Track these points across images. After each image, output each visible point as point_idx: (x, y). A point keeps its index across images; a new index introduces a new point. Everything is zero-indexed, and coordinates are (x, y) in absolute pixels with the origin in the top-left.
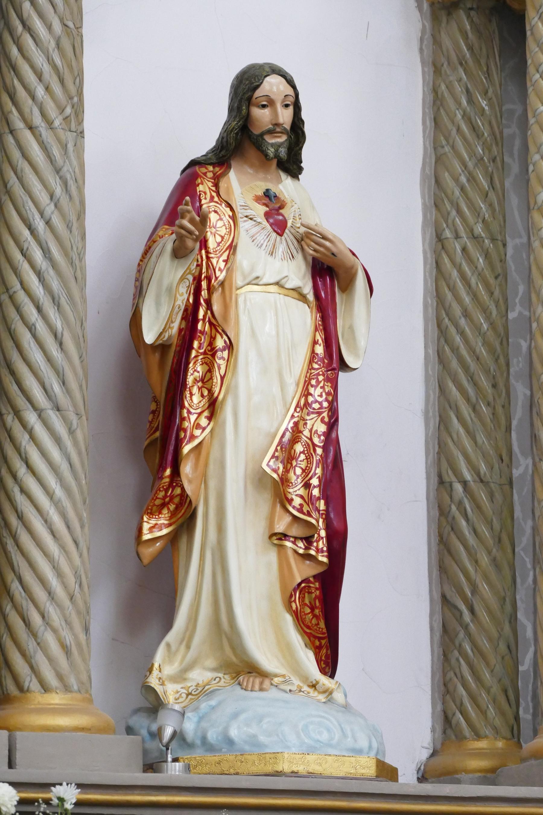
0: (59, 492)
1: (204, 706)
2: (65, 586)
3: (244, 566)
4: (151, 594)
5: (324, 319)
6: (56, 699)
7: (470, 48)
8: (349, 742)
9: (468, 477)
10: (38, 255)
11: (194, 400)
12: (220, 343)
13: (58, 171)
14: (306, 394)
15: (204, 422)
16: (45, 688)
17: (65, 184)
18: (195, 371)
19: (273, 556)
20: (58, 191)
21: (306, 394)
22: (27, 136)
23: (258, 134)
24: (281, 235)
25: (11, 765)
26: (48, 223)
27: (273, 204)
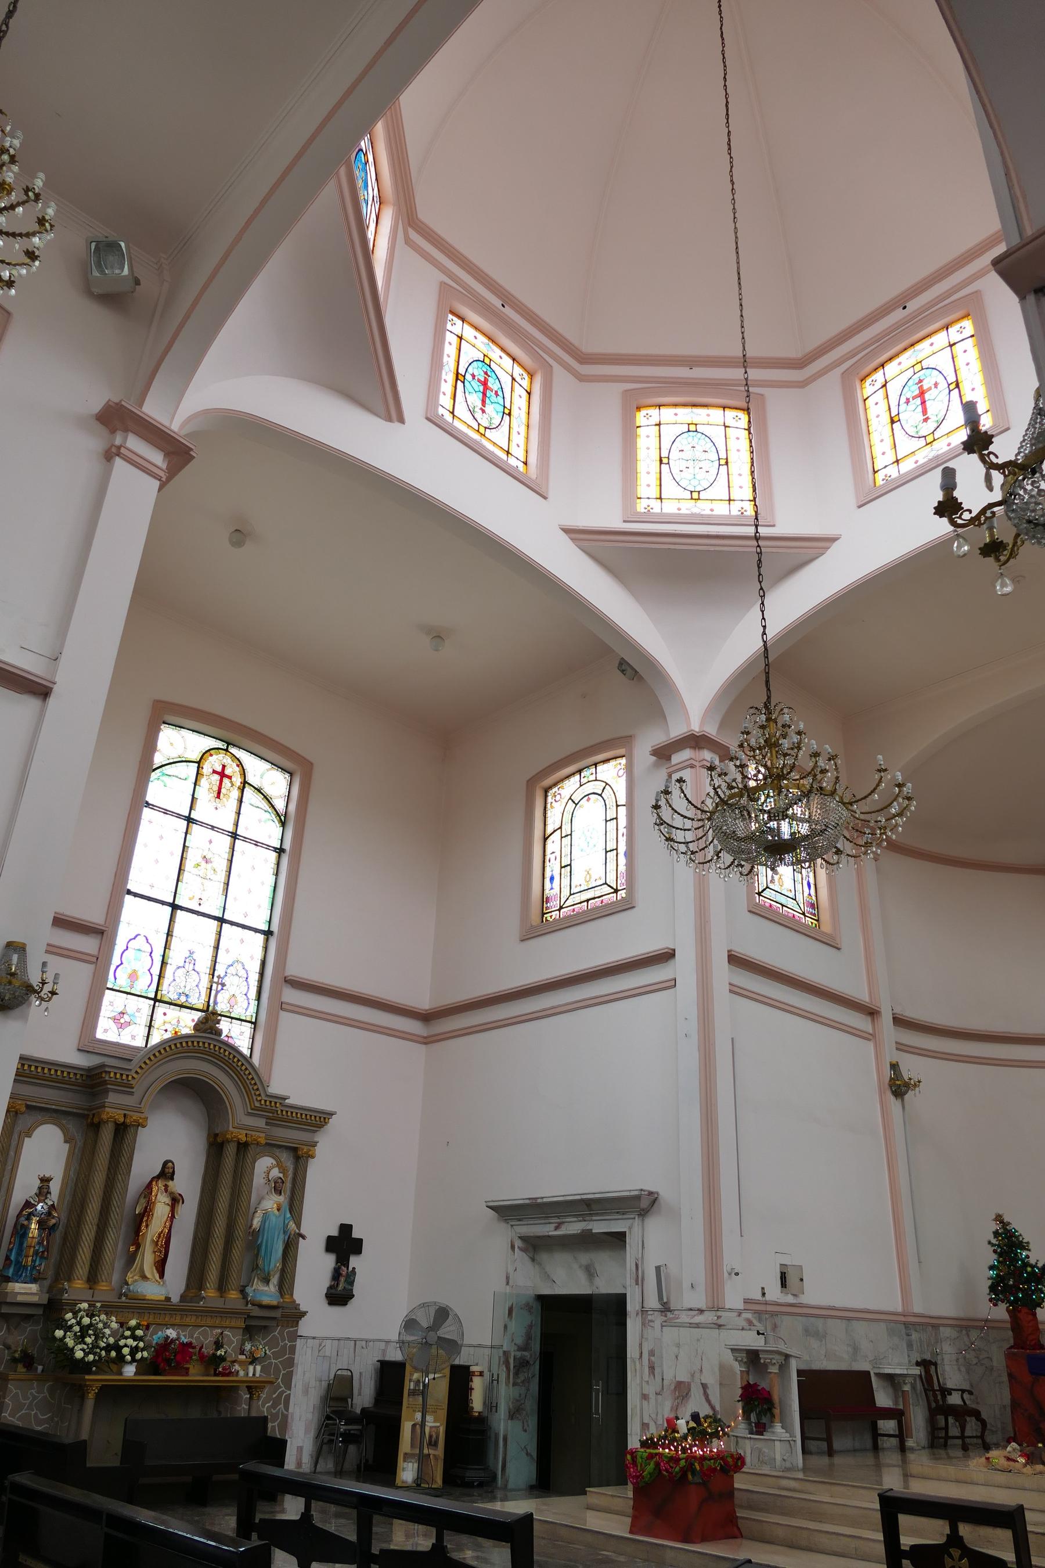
3: (148, 1258)
4: (131, 1259)
23: (167, 1173)
24: (617, 1304)
27: (166, 1186)
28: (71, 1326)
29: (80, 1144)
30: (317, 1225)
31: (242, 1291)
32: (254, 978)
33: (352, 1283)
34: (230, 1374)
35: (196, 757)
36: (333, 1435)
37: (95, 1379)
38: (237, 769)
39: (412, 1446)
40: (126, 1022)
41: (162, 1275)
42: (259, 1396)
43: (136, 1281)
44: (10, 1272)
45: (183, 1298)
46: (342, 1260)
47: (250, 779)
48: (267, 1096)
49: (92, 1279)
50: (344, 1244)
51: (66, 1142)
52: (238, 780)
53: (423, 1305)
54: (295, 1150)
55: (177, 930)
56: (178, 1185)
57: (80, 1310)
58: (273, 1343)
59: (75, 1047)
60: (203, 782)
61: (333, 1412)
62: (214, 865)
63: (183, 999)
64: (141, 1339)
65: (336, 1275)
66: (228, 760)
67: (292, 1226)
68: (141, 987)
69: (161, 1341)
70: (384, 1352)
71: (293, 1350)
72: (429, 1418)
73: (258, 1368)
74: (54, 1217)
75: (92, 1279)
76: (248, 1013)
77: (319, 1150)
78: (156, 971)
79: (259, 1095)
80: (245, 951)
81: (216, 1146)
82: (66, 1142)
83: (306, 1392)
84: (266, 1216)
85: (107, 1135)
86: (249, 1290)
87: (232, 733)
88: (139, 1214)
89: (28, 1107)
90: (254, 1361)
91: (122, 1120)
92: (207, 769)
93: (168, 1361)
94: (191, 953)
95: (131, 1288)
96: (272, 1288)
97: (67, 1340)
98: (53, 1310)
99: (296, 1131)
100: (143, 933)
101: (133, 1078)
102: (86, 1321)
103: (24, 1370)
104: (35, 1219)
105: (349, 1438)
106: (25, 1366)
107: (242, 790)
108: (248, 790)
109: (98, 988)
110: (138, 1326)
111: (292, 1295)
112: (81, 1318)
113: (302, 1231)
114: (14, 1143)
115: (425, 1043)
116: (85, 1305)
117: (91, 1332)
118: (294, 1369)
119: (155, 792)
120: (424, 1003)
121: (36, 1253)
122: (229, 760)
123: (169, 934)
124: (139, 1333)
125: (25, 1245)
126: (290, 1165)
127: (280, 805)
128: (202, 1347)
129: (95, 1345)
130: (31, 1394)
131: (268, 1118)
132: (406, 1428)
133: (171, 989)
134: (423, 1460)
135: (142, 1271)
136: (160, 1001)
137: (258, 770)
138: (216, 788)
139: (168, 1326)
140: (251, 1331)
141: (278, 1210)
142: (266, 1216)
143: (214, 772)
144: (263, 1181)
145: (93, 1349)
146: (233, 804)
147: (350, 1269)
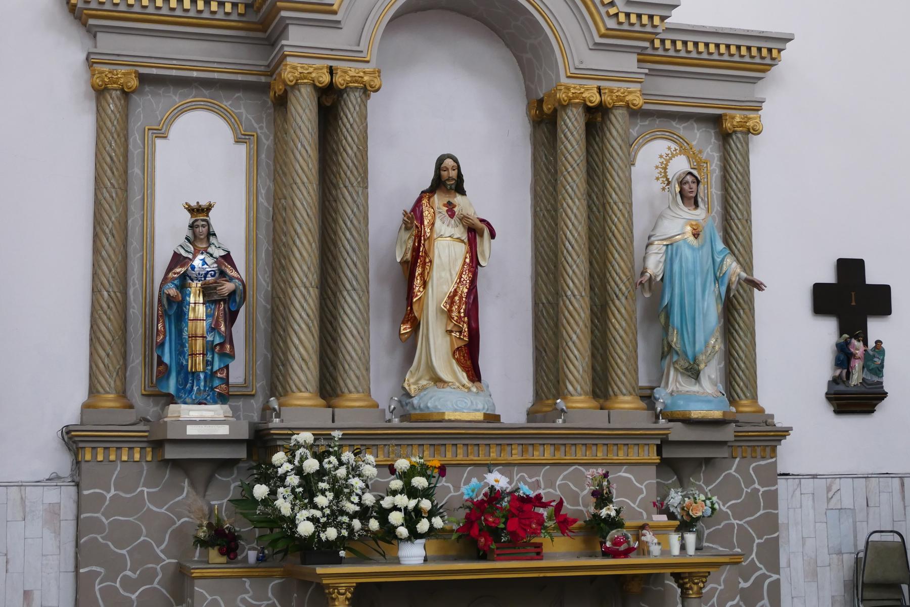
0: (355, 320)
1: (422, 394)
2: (357, 354)
3: (438, 343)
4: (409, 346)
5: (471, 248)
6: (355, 396)
7: (547, 138)
8: (474, 407)
9: (544, 301)
10: (348, 234)
11: (418, 282)
12: (427, 260)
13: (355, 202)
14: (460, 277)
15: (421, 289)
16: (350, 392)
17: (358, 206)
18: (418, 271)
19: (448, 338)
20: (355, 210)
21: (460, 277)
22: (345, 190)
23: (447, 181)
25: (333, 421)
26: (351, 221)
27: (451, 209)
28: (285, 475)
29: (267, 143)
30: (788, 267)
31: (648, 398)
33: (879, 370)
34: (626, 553)
41: (475, 374)
42: (699, 592)
43: (424, 388)
44: (172, 386)
45: (531, 415)
46: (852, 327)
49: (329, 388)
51: (238, 141)
54: (716, 121)
56: (476, 202)
57: (298, 446)
58: (728, 490)
64: (426, 493)
65: (843, 357)
67: (732, 267)
71: (772, 499)
73: (691, 538)
74: (231, 279)
75: (329, 388)
77: (767, 117)
81: (544, 121)
82: (238, 141)
83: (812, 574)
84: (671, 246)
85: (304, 112)
88: (404, 263)
89: (144, 79)
90: (686, 524)
91: (326, 79)
93: (495, 533)
95: (415, 401)
102: (311, 465)
103: (224, 559)
104: (195, 286)
106: (222, 553)
110: (413, 471)
111: (755, 398)
112: (302, 461)
113: (758, 276)
114: (135, 152)
117: (323, 485)
118: (782, 533)
121: (210, 348)
124: (419, 482)
126: (711, 152)
129: (336, 513)
130: (244, 601)
131: (639, 54)
135: (430, 368)
139: (490, 467)
140: (675, 465)
141: (696, 235)
142: (671, 246)
144: (658, 185)
145: (334, 516)
147: (871, 344)
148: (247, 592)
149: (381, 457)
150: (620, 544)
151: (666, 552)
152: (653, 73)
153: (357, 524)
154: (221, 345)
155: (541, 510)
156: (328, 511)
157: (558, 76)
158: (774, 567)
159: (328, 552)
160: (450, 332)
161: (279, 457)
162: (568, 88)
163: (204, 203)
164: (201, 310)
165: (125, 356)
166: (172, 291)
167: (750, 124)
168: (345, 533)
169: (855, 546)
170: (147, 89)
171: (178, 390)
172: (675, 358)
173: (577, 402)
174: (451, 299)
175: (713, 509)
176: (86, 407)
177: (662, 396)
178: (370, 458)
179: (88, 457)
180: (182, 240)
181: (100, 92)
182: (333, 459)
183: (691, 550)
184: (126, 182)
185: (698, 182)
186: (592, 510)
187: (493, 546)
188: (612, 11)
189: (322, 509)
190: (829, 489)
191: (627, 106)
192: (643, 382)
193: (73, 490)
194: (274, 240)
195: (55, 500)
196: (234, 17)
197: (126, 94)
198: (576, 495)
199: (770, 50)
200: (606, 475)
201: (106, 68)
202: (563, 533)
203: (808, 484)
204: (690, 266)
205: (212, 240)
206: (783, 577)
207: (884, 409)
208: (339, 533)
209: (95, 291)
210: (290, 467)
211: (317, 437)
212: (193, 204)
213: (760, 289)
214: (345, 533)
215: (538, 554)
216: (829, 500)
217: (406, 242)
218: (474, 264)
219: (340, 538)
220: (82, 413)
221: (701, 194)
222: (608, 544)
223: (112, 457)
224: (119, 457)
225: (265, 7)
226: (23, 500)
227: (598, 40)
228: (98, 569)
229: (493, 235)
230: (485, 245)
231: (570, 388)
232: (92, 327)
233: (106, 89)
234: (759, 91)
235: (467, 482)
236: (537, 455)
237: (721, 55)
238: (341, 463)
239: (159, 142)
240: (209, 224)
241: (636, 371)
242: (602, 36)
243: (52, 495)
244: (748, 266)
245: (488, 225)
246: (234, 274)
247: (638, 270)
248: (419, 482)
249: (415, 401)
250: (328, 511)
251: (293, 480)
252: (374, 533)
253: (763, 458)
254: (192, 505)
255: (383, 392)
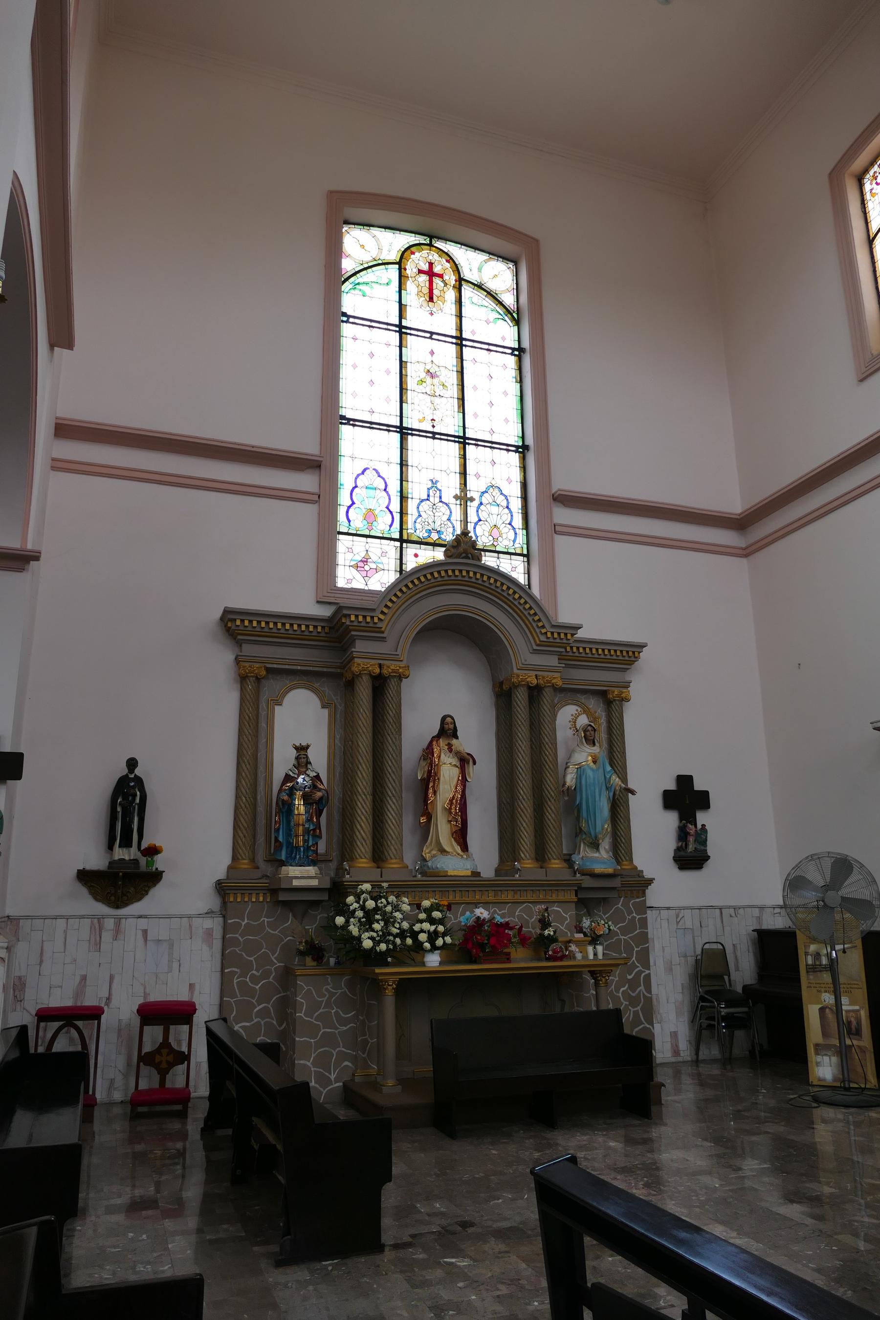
3: (443, 829)
4: (425, 831)
18: (431, 785)
23: (448, 730)
27: (450, 747)
28: (354, 911)
29: (340, 708)
30: (648, 780)
31: (568, 861)
32: (516, 504)
33: (704, 843)
34: (561, 958)
35: (394, 256)
36: (713, 1018)
37: (390, 973)
38: (448, 265)
39: (825, 1034)
40: (367, 566)
41: (465, 847)
42: (606, 982)
43: (434, 856)
45: (498, 871)
47: (467, 274)
48: (553, 626)
49: (378, 857)
50: (686, 799)
51: (323, 707)
52: (451, 278)
53: (811, 858)
54: (603, 695)
55: (411, 459)
56: (466, 742)
57: (363, 892)
59: (314, 602)
60: (410, 286)
61: (707, 992)
62: (442, 379)
63: (435, 536)
64: (441, 922)
65: (683, 835)
66: (434, 257)
67: (616, 780)
68: (382, 524)
69: (471, 922)
70: (759, 919)
71: (644, 923)
72: (845, 1000)
73: (600, 949)
74: (320, 790)
75: (378, 857)
76: (517, 545)
78: (395, 507)
79: (543, 627)
80: (497, 472)
82: (323, 707)
83: (670, 970)
84: (580, 769)
85: (364, 691)
86: (575, 858)
87: (433, 221)
88: (422, 780)
89: (268, 670)
90: (595, 940)
91: (377, 671)
92: (410, 269)
93: (481, 946)
94: (434, 483)
95: (430, 864)
96: (604, 852)
97: (351, 928)
98: (336, 893)
99: (602, 673)
100: (372, 465)
101: (379, 619)
102: (370, 904)
103: (315, 964)
104: (299, 794)
105: (733, 1023)
106: (314, 960)
107: (459, 289)
108: (467, 292)
109: (327, 534)
110: (435, 907)
111: (631, 860)
112: (365, 901)
113: (631, 785)
114: (263, 713)
115: (746, 556)
116: (367, 886)
117: (378, 917)
118: (650, 945)
119: (350, 302)
120: (735, 506)
121: (307, 832)
122: (436, 256)
123: (403, 464)
124: (437, 914)
125: (292, 824)
126: (601, 712)
127: (509, 300)
128: (521, 927)
130: (327, 990)
132: (812, 1013)
133: (418, 526)
134: (844, 1054)
135: (438, 843)
136: (408, 541)
137: (471, 262)
138: (426, 290)
139: (476, 905)
141: (595, 762)
142: (580, 769)
143: (420, 272)
144: (570, 733)
145: (385, 935)
146: (451, 308)
148: (328, 984)
149: (410, 899)
150: (558, 952)
151: (586, 957)
152: (568, 666)
153: (398, 941)
154: (314, 830)
155: (511, 933)
156: (381, 933)
157: (512, 669)
158: (647, 966)
159: (379, 959)
160: (450, 822)
161: (350, 899)
162: (518, 676)
163: (304, 744)
164: (302, 808)
165: (254, 837)
166: (286, 798)
167: (624, 695)
168: (391, 947)
169: (695, 952)
170: (270, 676)
171: (287, 858)
172: (584, 836)
173: (527, 863)
174: (451, 801)
175: (610, 930)
176: (230, 868)
177: (577, 859)
178: (406, 900)
179: (232, 899)
180: (291, 766)
181: (243, 679)
182: (383, 900)
183: (600, 956)
184: (257, 731)
185: (595, 730)
186: (539, 931)
187: (481, 955)
188: (543, 631)
189: (377, 932)
190: (677, 916)
191: (553, 686)
192: (565, 852)
193: (221, 920)
194: (344, 765)
195: (210, 926)
196: (323, 634)
197: (258, 679)
198: (528, 922)
199: (634, 653)
200: (546, 910)
201: (247, 664)
202: (523, 946)
203: (664, 913)
204: (592, 781)
205: (309, 766)
206: (652, 972)
207: (709, 865)
208: (387, 946)
209: (238, 797)
210: (358, 905)
211: (373, 887)
212: (298, 745)
213: (633, 794)
214: (391, 947)
215: (508, 959)
216: (678, 923)
217: (424, 767)
218: (464, 781)
219: (388, 950)
220: (228, 872)
221: (597, 737)
222: (550, 953)
223: (246, 899)
224: (250, 899)
225: (341, 630)
226: (190, 926)
227: (535, 647)
228: (236, 970)
229: (474, 763)
230: (471, 770)
231: (522, 855)
232: (235, 819)
233: (247, 676)
234: (628, 676)
235: (463, 914)
236: (504, 897)
237: (605, 655)
238: (388, 903)
239: (277, 707)
240: (307, 757)
241: (562, 845)
242: (538, 645)
243: (208, 923)
244: (624, 779)
245: (472, 756)
246: (322, 787)
247: (561, 783)
248: (437, 914)
249: (430, 864)
250: (381, 933)
251: (359, 914)
252: (409, 947)
253: (638, 897)
254: (291, 930)
255: (409, 858)
